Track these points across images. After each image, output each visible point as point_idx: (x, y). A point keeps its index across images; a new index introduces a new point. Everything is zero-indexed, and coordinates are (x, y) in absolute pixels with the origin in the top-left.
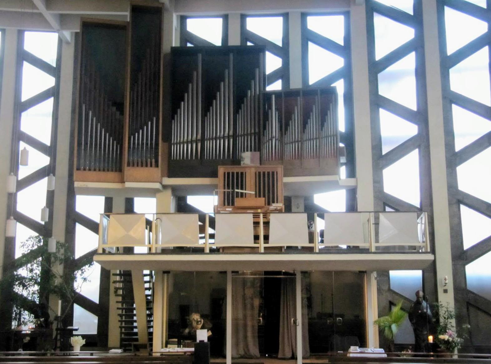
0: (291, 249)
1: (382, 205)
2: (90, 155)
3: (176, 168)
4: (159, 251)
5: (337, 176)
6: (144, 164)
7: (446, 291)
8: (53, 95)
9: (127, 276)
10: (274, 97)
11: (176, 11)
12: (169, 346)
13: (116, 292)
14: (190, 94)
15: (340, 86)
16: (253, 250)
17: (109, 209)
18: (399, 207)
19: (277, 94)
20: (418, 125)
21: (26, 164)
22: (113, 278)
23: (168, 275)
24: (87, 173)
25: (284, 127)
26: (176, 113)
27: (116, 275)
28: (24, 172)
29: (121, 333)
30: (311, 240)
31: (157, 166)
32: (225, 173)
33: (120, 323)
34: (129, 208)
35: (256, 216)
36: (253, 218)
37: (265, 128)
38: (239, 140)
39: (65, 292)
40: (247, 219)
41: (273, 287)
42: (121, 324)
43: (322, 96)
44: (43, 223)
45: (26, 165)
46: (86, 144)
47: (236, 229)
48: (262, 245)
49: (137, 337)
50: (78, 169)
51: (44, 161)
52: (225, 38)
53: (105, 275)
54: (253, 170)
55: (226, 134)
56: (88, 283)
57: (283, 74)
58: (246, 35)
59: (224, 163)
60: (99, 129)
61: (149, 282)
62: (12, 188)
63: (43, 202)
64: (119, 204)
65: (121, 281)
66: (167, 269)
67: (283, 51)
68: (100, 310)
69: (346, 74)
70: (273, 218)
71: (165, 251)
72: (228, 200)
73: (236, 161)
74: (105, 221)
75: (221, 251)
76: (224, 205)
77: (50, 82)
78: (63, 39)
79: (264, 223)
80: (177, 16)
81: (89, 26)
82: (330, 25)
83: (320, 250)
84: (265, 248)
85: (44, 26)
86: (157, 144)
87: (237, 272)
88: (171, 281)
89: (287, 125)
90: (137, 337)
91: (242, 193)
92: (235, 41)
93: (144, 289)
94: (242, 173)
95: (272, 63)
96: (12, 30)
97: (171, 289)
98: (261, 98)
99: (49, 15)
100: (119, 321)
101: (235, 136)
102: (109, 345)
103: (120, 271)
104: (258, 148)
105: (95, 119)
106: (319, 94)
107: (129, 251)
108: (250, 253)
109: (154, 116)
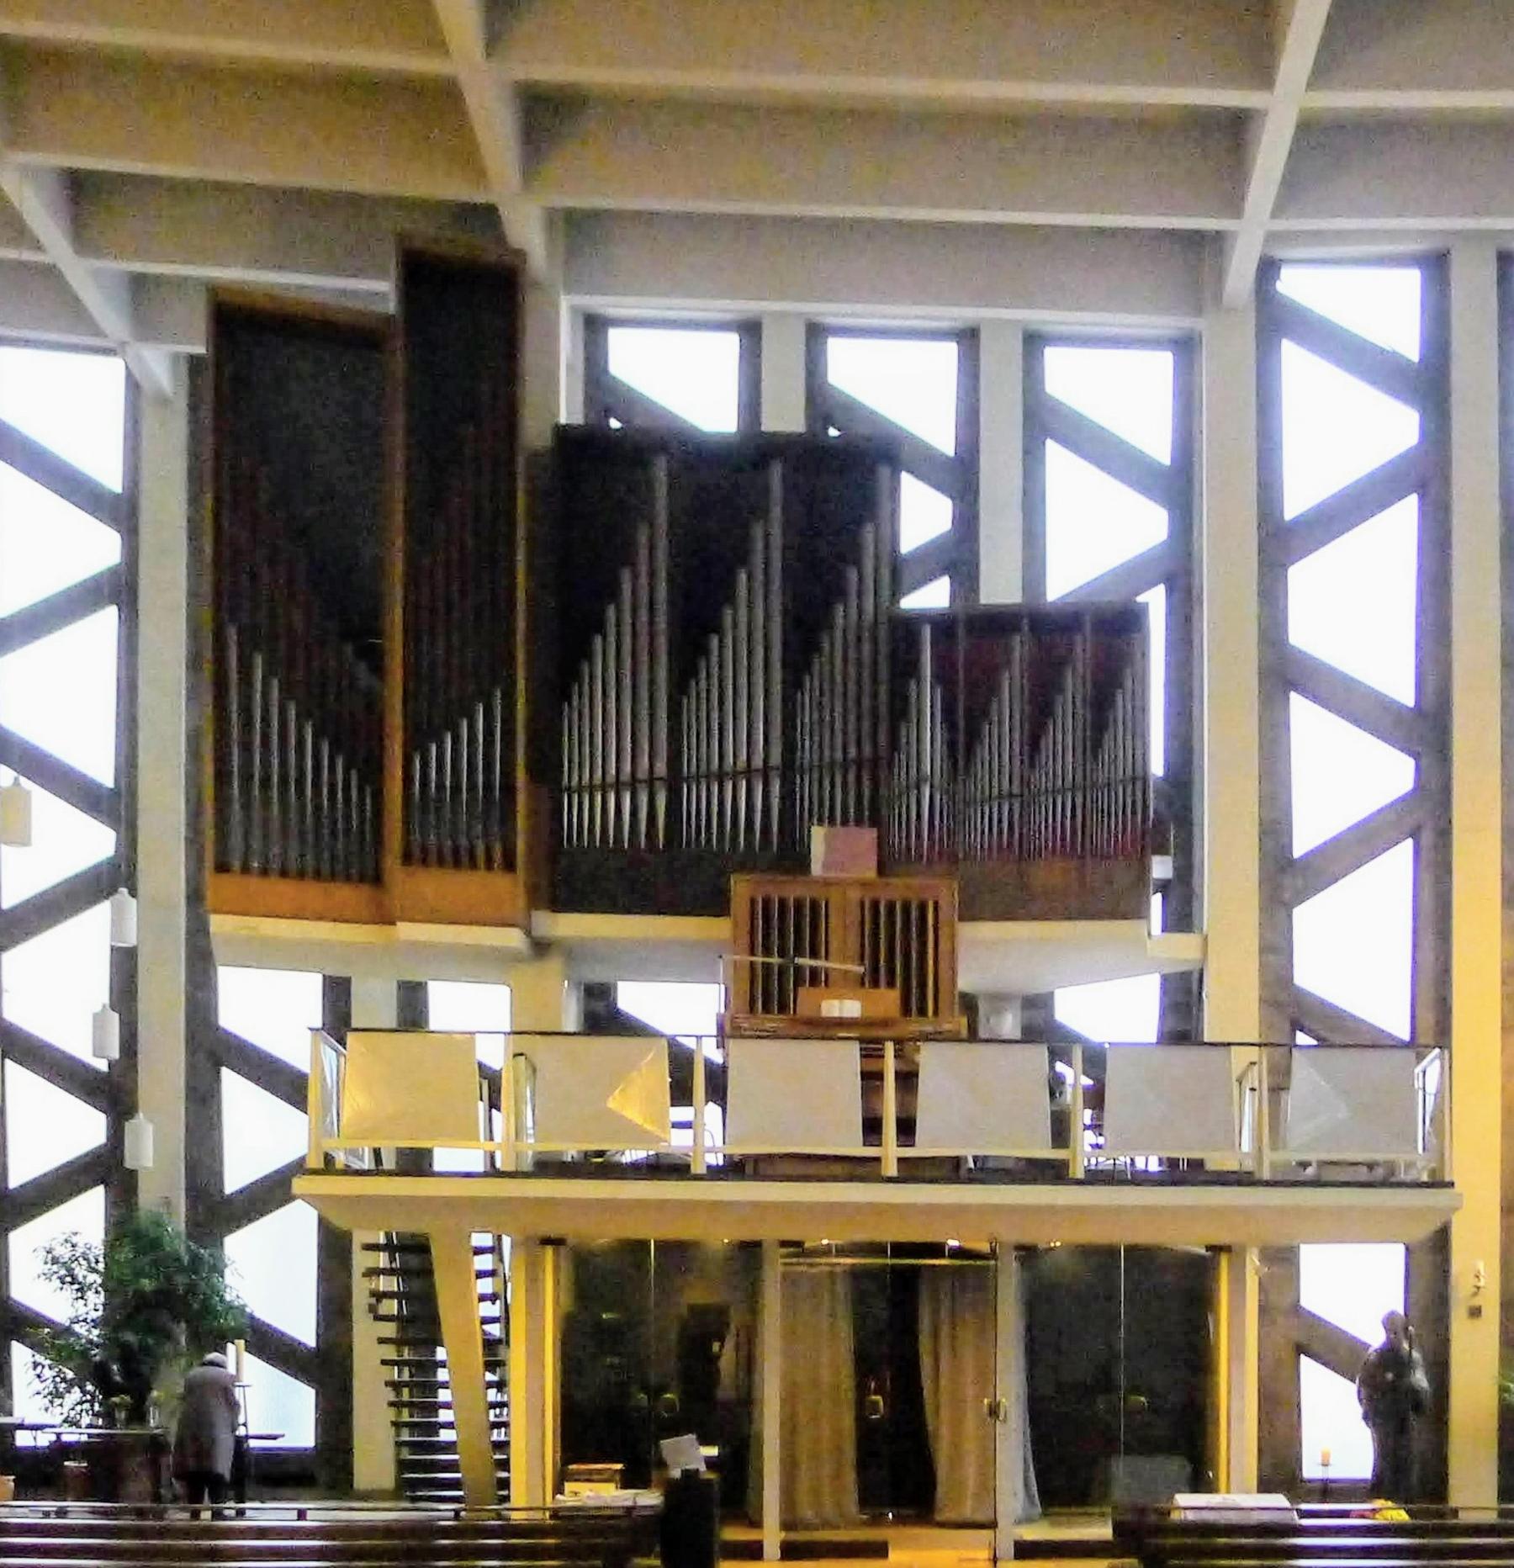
0: (986, 1172)
1: (1287, 1027)
2: (266, 822)
3: (577, 877)
4: (527, 1165)
5: (1143, 922)
6: (460, 859)
8: (114, 598)
9: (413, 1256)
13: (372, 1309)
14: (612, 639)
15: (1155, 601)
16: (861, 1169)
17: (338, 1021)
18: (1337, 1031)
19: (944, 625)
22: (361, 1261)
23: (556, 1254)
24: (254, 883)
25: (963, 742)
32: (753, 902)
33: (392, 1412)
34: (412, 1011)
35: (871, 1052)
36: (862, 1056)
37: (894, 745)
38: (806, 787)
39: (51, 1470)
42: (399, 1413)
44: (102, 1065)
45: (25, 841)
46: (246, 778)
47: (806, 1091)
48: (891, 1151)
49: (456, 1457)
50: (222, 867)
52: (751, 403)
53: (334, 1249)
54: (854, 895)
56: (269, 1272)
57: (958, 556)
58: (820, 401)
59: (746, 864)
63: (95, 985)
65: (397, 1279)
68: (325, 1367)
70: (929, 1058)
71: (548, 1167)
73: (794, 858)
75: (749, 1169)
76: (752, 1009)
78: (145, 385)
79: (899, 1075)
80: (574, 310)
81: (238, 325)
82: (1119, 384)
86: (509, 789)
88: (566, 1266)
89: (973, 736)
90: (456, 1457)
91: (814, 972)
92: (785, 416)
94: (815, 905)
95: (920, 515)
97: (567, 1302)
98: (883, 632)
100: (392, 1404)
101: (789, 768)
103: (388, 1236)
105: (275, 683)
106: (1088, 627)
107: (416, 1163)
108: (851, 1178)
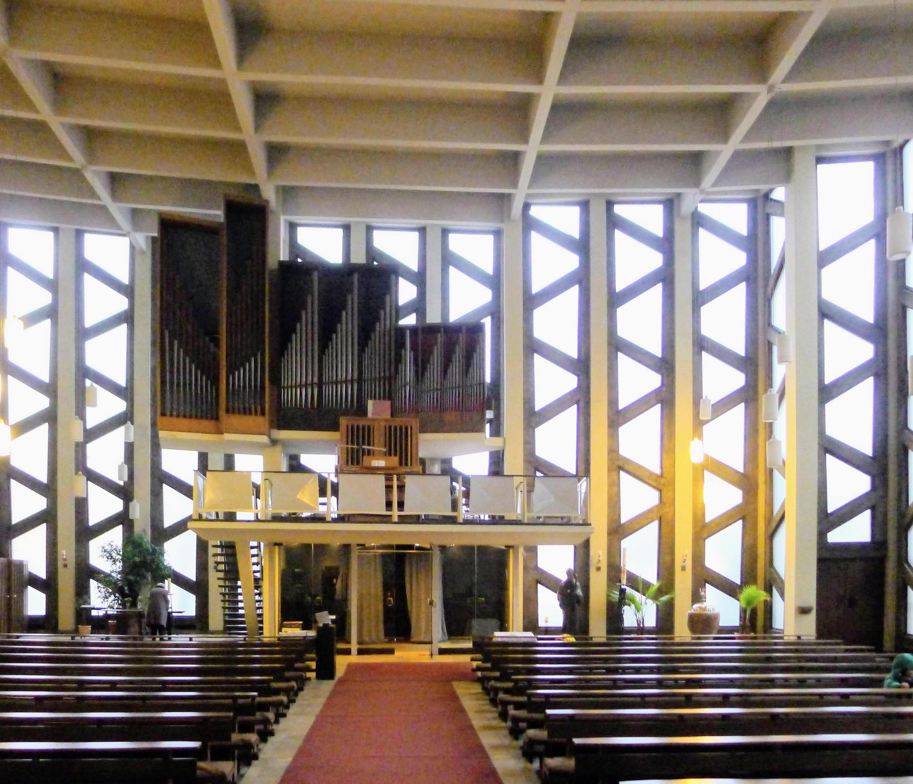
0: (429, 520)
2: (178, 398)
3: (286, 418)
4: (269, 518)
6: (246, 411)
7: (598, 569)
9: (229, 549)
11: (284, 214)
12: (284, 629)
15: (487, 322)
17: (203, 467)
18: (550, 471)
19: (414, 330)
20: (578, 376)
21: (94, 405)
22: (212, 551)
24: (175, 420)
26: (287, 348)
28: (94, 417)
29: (225, 615)
30: (454, 506)
31: (263, 414)
32: (348, 426)
34: (229, 464)
35: (389, 478)
38: (366, 387)
40: (379, 481)
43: (470, 333)
44: (121, 483)
47: (366, 493)
48: (395, 513)
51: (119, 406)
53: (202, 547)
56: (180, 555)
57: (419, 306)
60: (188, 365)
61: (257, 555)
62: (80, 438)
67: (419, 278)
69: (495, 311)
70: (409, 481)
71: (276, 518)
72: (354, 460)
73: (361, 411)
74: (200, 480)
75: (346, 519)
77: (121, 303)
79: (398, 487)
80: (285, 221)
82: (475, 246)
85: (109, 225)
86: (263, 387)
87: (363, 545)
89: (424, 369)
91: (369, 451)
92: (358, 258)
93: (496, 480)
94: (369, 428)
95: (406, 292)
96: (68, 228)
97: (283, 565)
99: (118, 210)
101: (360, 380)
104: (389, 396)
107: (231, 517)
109: (258, 350)
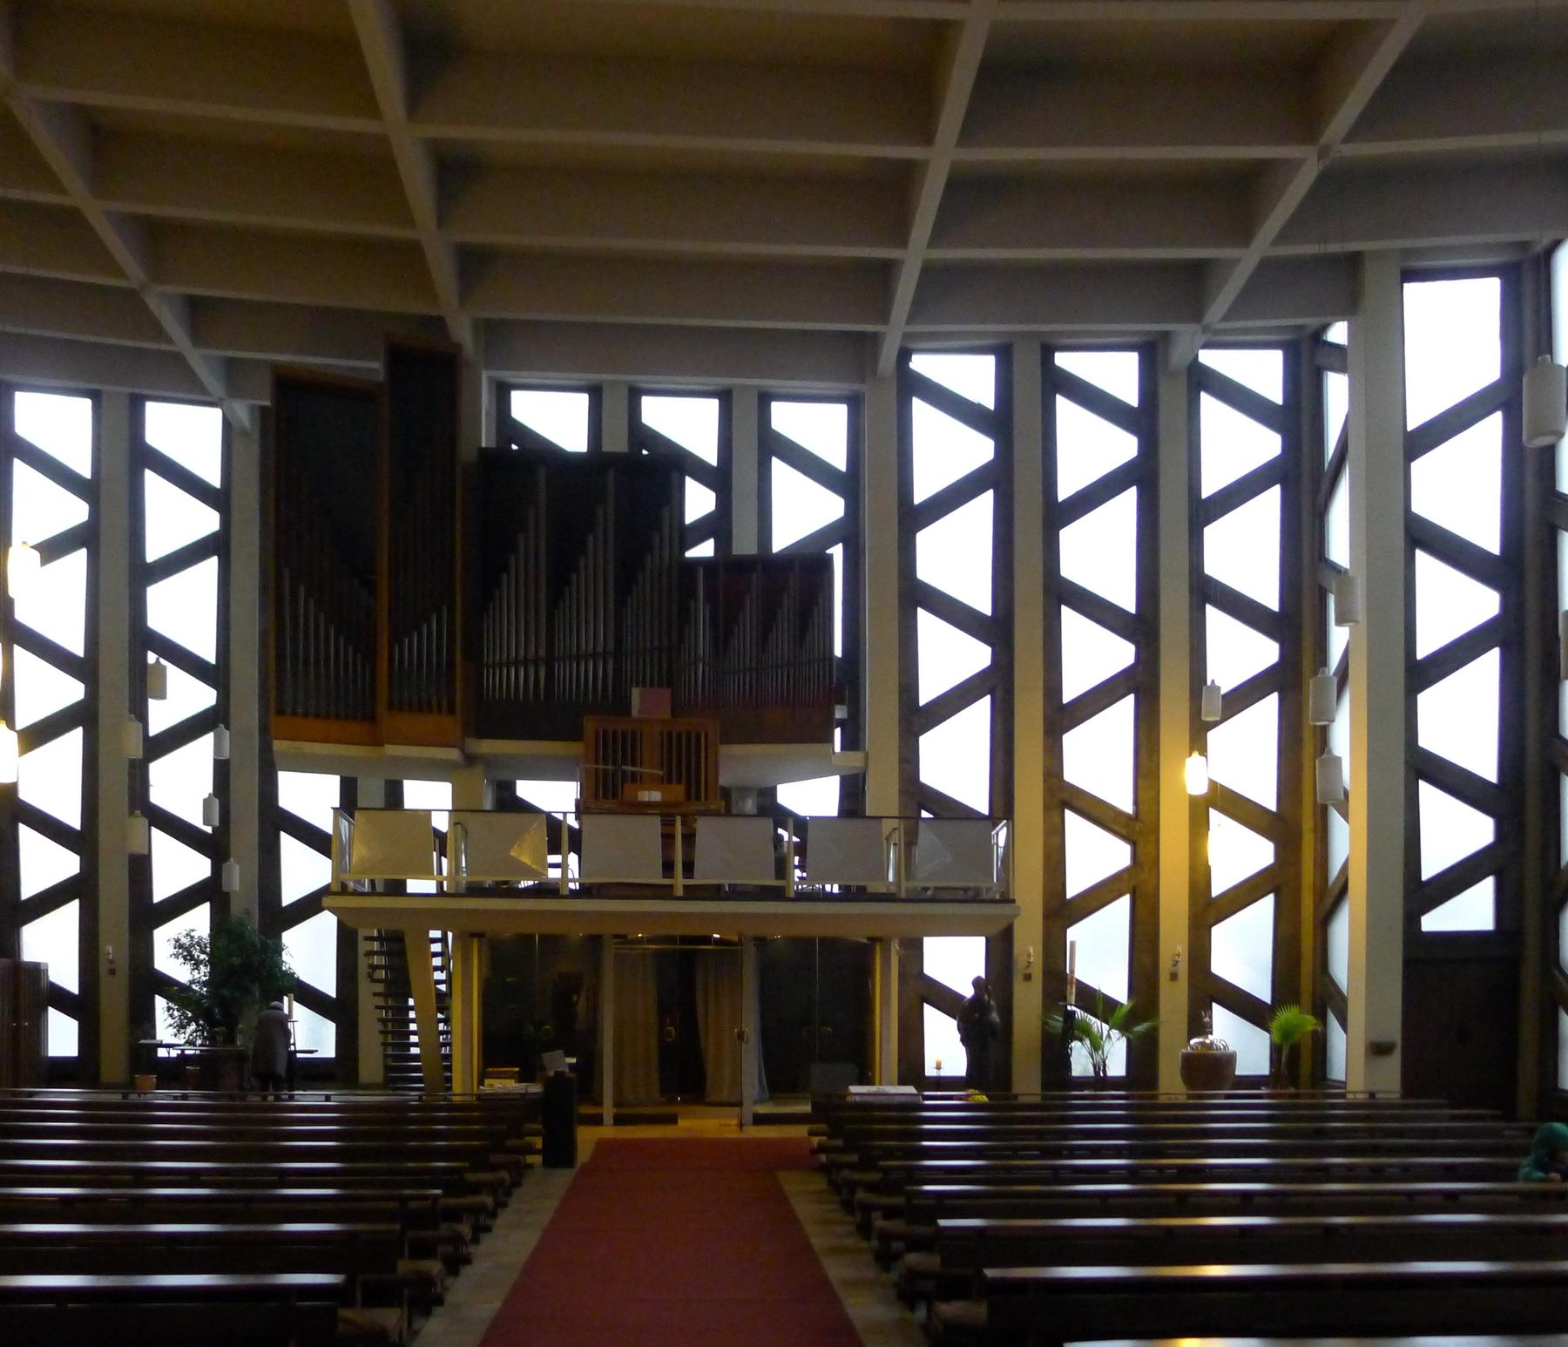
6: (423, 707)
7: (1028, 977)
10: (701, 571)
11: (489, 366)
13: (370, 976)
15: (837, 552)
17: (349, 804)
22: (363, 946)
27: (371, 939)
28: (162, 716)
30: (782, 869)
31: (452, 711)
32: (597, 732)
35: (667, 823)
40: (651, 827)
41: (684, 968)
44: (209, 829)
48: (679, 881)
50: (280, 712)
55: (600, 649)
57: (716, 525)
58: (641, 435)
62: (136, 751)
64: (372, 792)
66: (477, 928)
69: (847, 531)
70: (703, 827)
73: (621, 705)
77: (207, 521)
80: (490, 379)
82: (817, 425)
83: (797, 892)
84: (685, 887)
85: (194, 393)
86: (451, 665)
91: (633, 774)
92: (616, 443)
95: (698, 501)
99: (199, 360)
102: (737, 749)
103: (379, 932)
107: (397, 888)
